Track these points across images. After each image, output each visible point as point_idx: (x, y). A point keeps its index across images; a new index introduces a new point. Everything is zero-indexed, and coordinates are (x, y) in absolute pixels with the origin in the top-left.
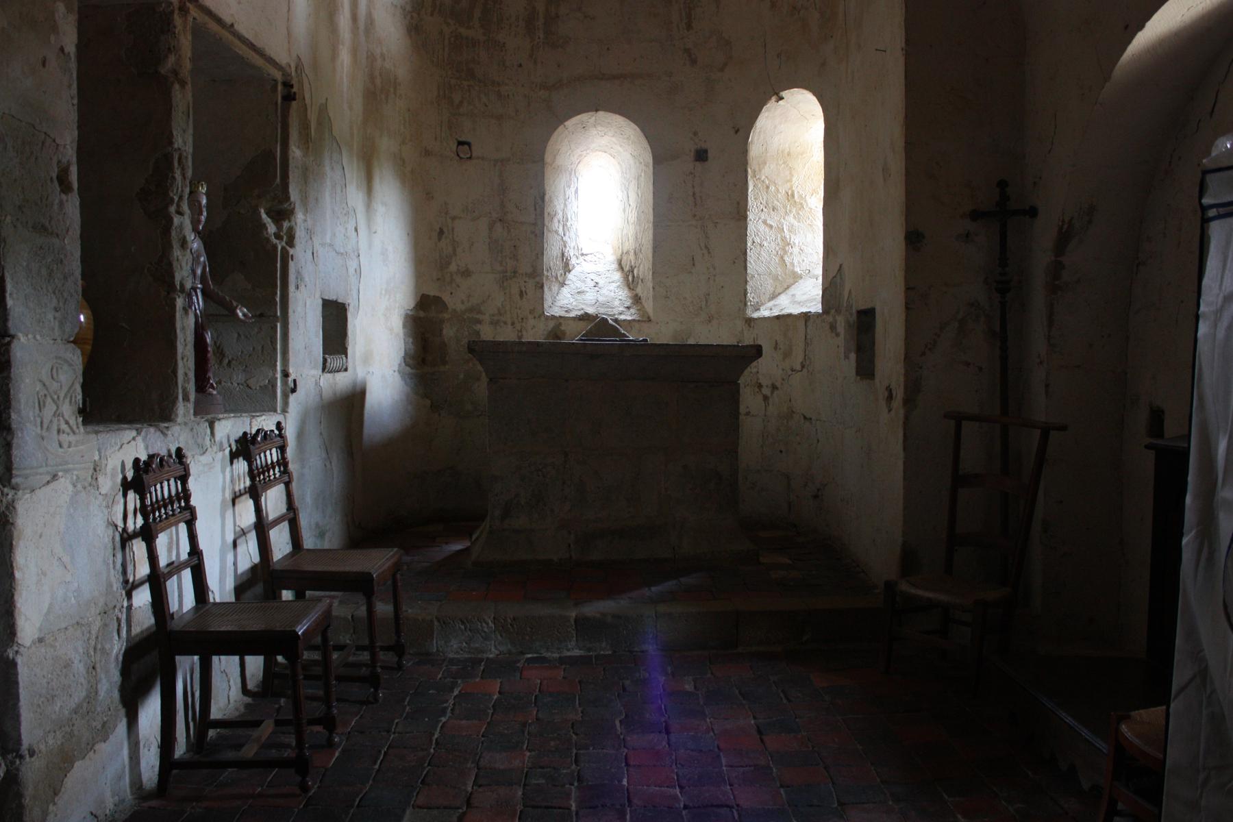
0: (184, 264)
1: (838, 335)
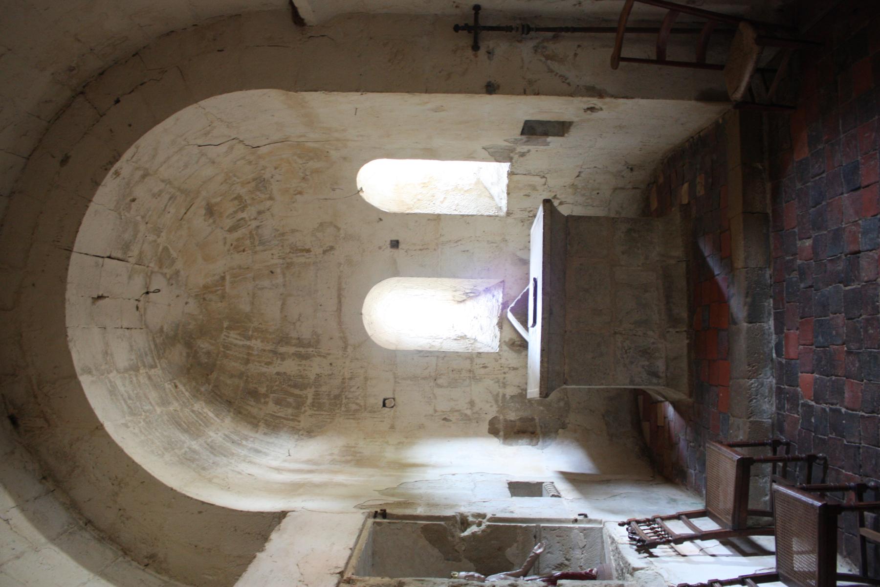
1: (529, 151)
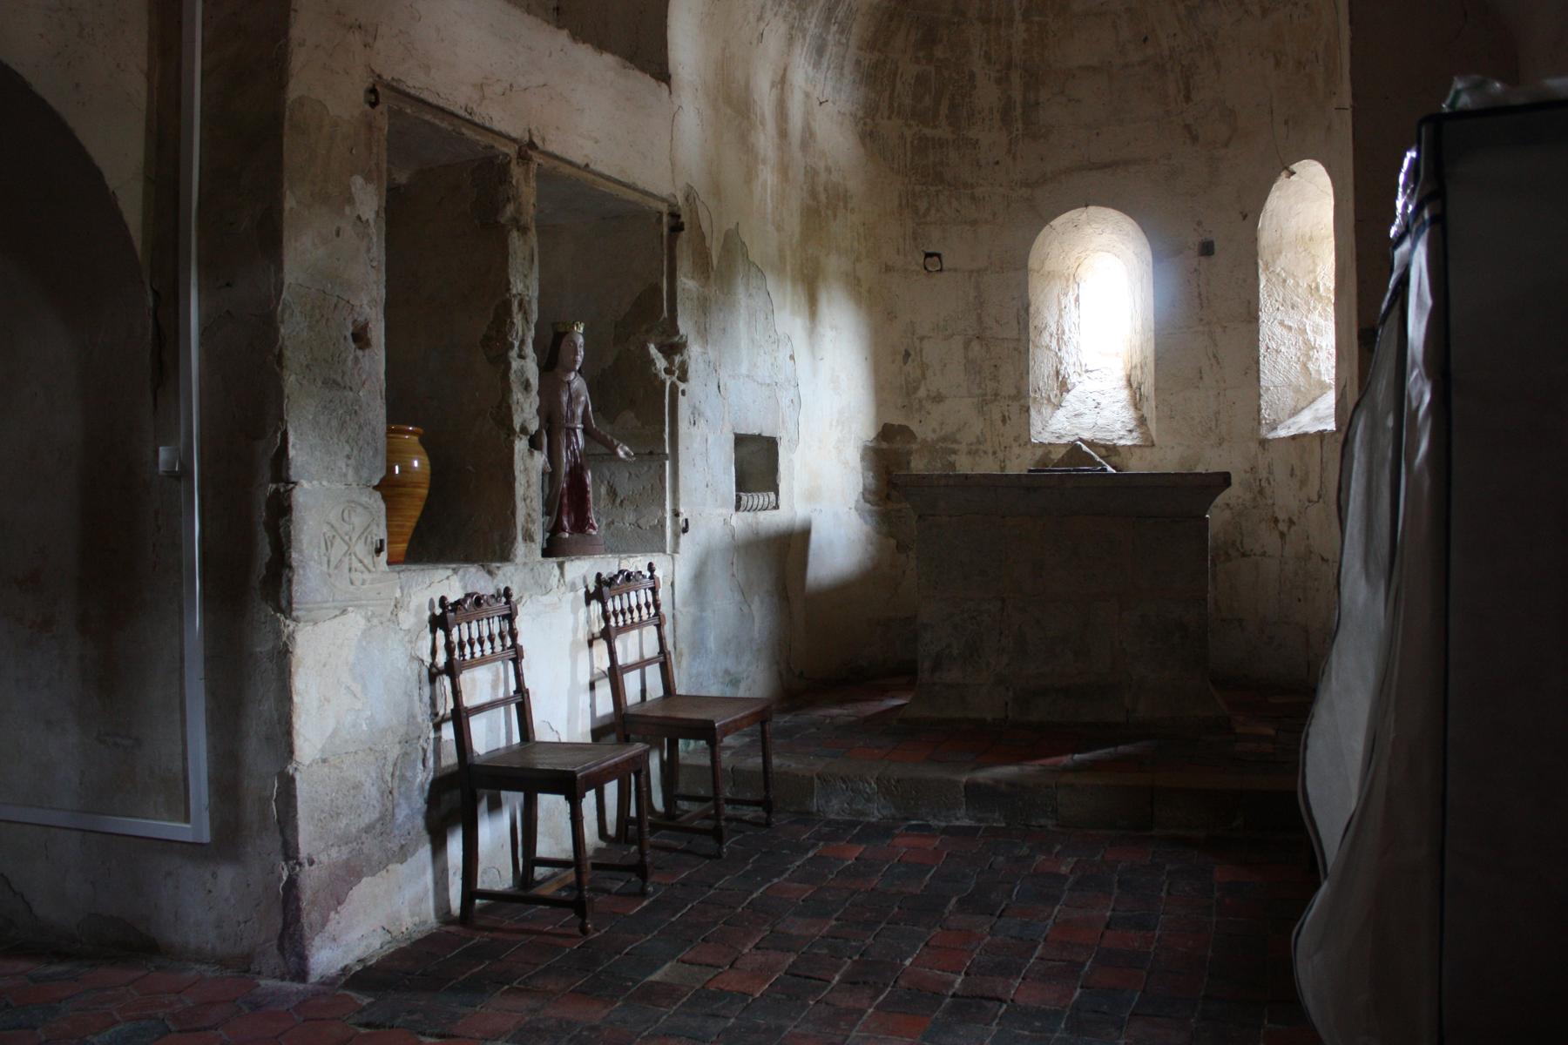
0: (526, 406)
